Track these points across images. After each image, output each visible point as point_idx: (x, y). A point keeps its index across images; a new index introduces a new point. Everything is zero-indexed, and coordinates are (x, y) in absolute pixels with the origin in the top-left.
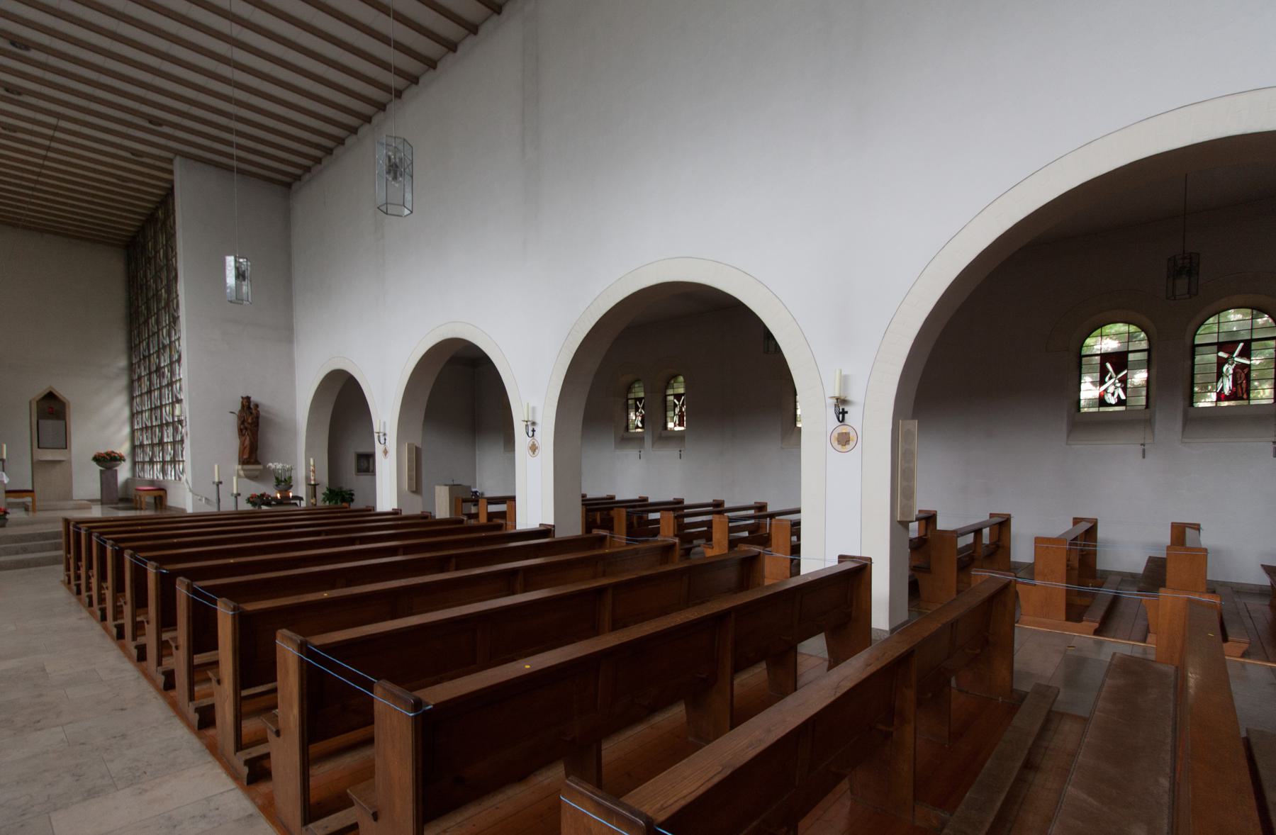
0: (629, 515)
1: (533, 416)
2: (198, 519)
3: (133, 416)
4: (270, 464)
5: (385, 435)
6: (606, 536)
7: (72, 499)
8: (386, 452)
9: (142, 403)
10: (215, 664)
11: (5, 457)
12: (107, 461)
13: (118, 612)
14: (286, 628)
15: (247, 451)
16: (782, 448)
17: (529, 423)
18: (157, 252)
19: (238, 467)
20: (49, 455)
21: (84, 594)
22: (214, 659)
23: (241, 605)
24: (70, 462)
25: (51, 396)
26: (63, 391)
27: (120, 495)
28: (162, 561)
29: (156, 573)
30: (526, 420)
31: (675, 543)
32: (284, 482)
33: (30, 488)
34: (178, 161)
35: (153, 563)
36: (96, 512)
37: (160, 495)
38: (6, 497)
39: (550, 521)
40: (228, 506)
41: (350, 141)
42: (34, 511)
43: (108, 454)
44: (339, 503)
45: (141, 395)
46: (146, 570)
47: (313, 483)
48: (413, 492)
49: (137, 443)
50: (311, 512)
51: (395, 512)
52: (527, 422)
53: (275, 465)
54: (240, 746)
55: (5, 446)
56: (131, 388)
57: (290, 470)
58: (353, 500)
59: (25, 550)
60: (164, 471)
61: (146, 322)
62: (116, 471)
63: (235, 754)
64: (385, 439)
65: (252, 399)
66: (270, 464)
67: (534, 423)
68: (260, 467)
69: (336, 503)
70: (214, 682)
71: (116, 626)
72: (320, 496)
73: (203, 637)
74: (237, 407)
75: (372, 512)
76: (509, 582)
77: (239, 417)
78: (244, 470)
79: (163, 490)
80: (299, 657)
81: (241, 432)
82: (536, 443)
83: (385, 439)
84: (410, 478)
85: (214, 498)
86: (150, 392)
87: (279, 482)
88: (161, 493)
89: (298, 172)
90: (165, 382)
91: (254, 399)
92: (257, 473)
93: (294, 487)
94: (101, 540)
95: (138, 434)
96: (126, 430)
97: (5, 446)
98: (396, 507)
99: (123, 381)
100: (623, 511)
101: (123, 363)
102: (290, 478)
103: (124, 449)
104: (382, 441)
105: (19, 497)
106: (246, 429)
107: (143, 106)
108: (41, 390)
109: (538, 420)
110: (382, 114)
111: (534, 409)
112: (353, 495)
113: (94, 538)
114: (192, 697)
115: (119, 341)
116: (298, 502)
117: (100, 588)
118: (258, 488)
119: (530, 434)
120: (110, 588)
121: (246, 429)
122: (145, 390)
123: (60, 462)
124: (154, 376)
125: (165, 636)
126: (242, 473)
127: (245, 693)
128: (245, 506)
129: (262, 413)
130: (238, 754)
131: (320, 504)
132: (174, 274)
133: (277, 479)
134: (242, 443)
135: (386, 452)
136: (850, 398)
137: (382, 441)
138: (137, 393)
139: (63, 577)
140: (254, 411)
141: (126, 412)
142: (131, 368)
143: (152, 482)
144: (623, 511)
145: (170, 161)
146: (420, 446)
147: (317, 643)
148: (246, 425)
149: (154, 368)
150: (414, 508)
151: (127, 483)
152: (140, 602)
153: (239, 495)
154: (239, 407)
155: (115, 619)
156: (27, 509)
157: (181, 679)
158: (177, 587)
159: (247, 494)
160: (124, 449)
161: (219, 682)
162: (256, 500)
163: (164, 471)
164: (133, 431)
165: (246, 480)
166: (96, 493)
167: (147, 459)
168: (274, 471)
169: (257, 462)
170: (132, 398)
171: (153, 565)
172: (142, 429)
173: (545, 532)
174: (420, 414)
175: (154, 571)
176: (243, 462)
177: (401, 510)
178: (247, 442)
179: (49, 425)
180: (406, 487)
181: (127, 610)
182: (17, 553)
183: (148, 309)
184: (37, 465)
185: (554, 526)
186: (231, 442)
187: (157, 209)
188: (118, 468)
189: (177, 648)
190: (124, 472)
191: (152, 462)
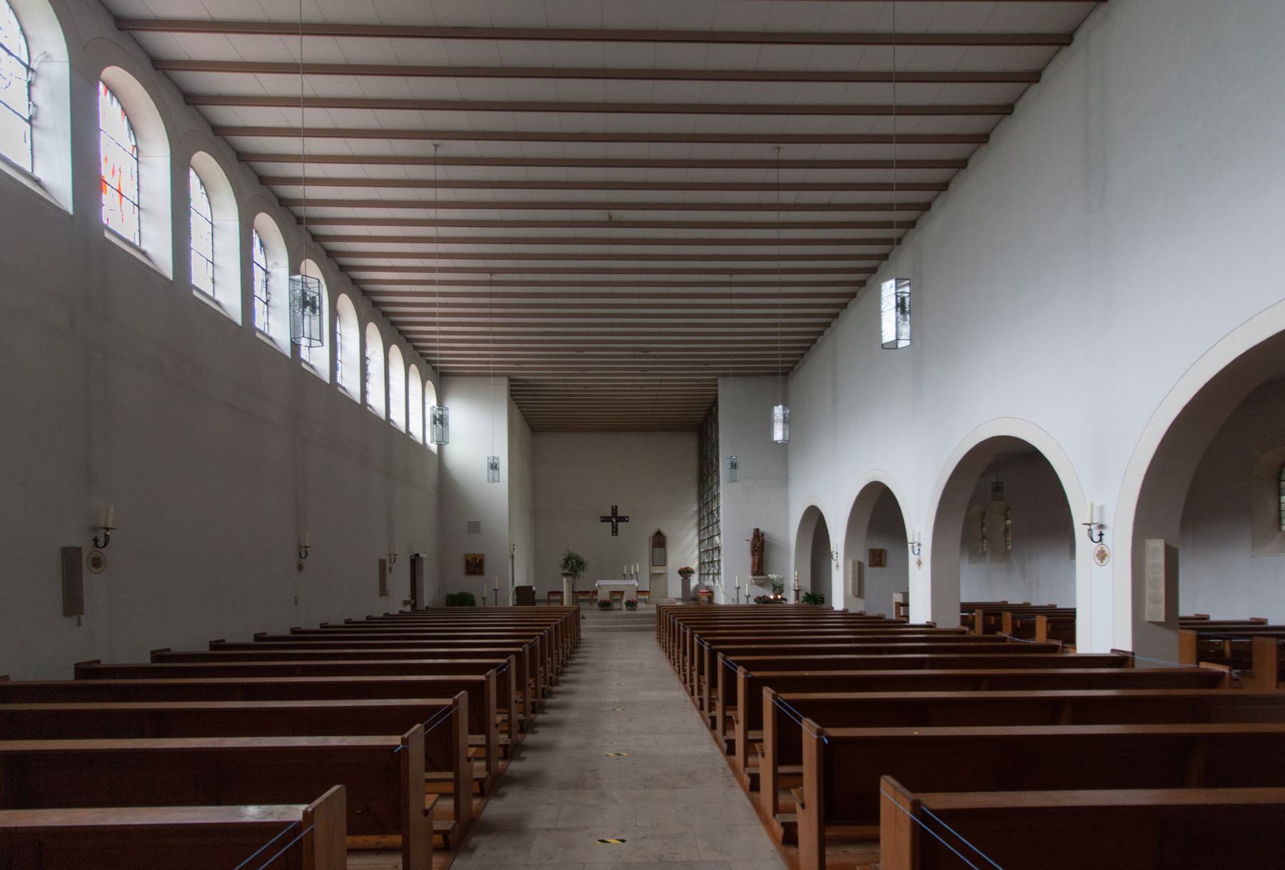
0: (1014, 619)
1: (919, 539)
2: (726, 608)
3: (701, 542)
4: (770, 575)
5: (837, 553)
6: (1223, 674)
7: (667, 598)
8: (919, 563)
9: (713, 530)
10: (761, 741)
11: (625, 573)
12: (685, 573)
13: (700, 691)
14: (811, 718)
15: (756, 566)
16: (1253, 556)
17: (1093, 527)
18: (712, 435)
19: (751, 577)
20: (658, 570)
21: (676, 665)
22: (759, 737)
23: (825, 729)
24: (666, 574)
25: (659, 534)
26: (665, 531)
27: (692, 595)
28: (749, 666)
29: (745, 679)
30: (1089, 522)
31: (1059, 646)
32: (778, 588)
33: (648, 590)
34: (721, 380)
35: (707, 643)
36: (680, 603)
37: (711, 594)
38: (637, 595)
39: (1126, 645)
40: (743, 602)
41: (820, 340)
42: (649, 604)
43: (686, 569)
44: (813, 604)
45: (704, 529)
46: (736, 674)
47: (797, 588)
48: (856, 596)
49: (702, 561)
50: (796, 607)
51: (929, 625)
52: (1090, 525)
53: (773, 576)
54: (776, 810)
55: (625, 567)
56: (699, 524)
57: (782, 579)
58: (823, 602)
59: (643, 623)
60: (714, 580)
61: (707, 480)
62: (689, 580)
63: (774, 816)
64: (919, 550)
65: (760, 530)
66: (770, 575)
67: (1101, 526)
68: (764, 577)
69: (811, 604)
70: (760, 756)
71: (711, 717)
72: (801, 599)
73: (754, 721)
74: (751, 536)
75: (907, 624)
76: (1053, 711)
77: (752, 543)
78: (754, 579)
79: (711, 592)
80: (911, 818)
81: (753, 552)
82: (1105, 548)
83: (919, 550)
84: (853, 585)
85: (736, 598)
86: (708, 527)
87: (775, 588)
88: (711, 594)
89: (791, 365)
90: (715, 521)
91: (762, 529)
92: (762, 581)
93: (785, 592)
94: (700, 641)
95: (702, 554)
96: (696, 553)
97: (625, 567)
98: (930, 620)
99: (695, 521)
100: (1272, 643)
101: (695, 508)
102: (782, 585)
103: (694, 565)
104: (916, 552)
105: (643, 595)
106: (756, 551)
107: (729, 292)
108: (654, 531)
109: (1108, 522)
110: (836, 320)
111: (1102, 508)
112: (823, 598)
113: (696, 640)
114: (746, 764)
115: (693, 493)
116: (784, 602)
117: (699, 680)
118: (761, 592)
119: (1096, 538)
120: (696, 670)
121: (756, 551)
122: (706, 526)
123: (662, 574)
124: (710, 516)
125: (729, 713)
126: (753, 581)
127: (782, 770)
128: (752, 602)
129: (765, 539)
130: (777, 815)
131: (801, 603)
132: (715, 454)
133: (774, 585)
134: (754, 561)
135: (919, 563)
136: (1104, 523)
137: (916, 552)
138: (702, 528)
139: (656, 636)
140: (761, 539)
141: (696, 541)
142: (700, 511)
143: (708, 587)
144: (1272, 643)
145: (717, 379)
146: (862, 561)
147: (935, 807)
148: (756, 548)
149: (710, 511)
150: (858, 607)
151: (697, 588)
152: (730, 701)
153: (749, 596)
154: (752, 536)
155: (710, 710)
156: (646, 602)
157: (740, 748)
158: (881, 790)
159: (754, 596)
160: (694, 565)
161: (763, 755)
162: (762, 600)
163: (714, 580)
164: (700, 553)
165: (756, 586)
166: (680, 596)
167: (706, 572)
168: (772, 580)
169: (762, 574)
170: (700, 531)
171: (769, 691)
172: (704, 552)
173: (1119, 659)
174: (959, 526)
175: (816, 737)
176: (754, 574)
177: (935, 623)
178: (756, 560)
179: (658, 550)
180: (850, 592)
181: (719, 705)
182: (639, 624)
183: (708, 471)
184: (654, 576)
185: (1133, 653)
186: (747, 560)
187: (712, 406)
188: (691, 578)
189: (737, 722)
190: (694, 581)
191: (708, 574)
